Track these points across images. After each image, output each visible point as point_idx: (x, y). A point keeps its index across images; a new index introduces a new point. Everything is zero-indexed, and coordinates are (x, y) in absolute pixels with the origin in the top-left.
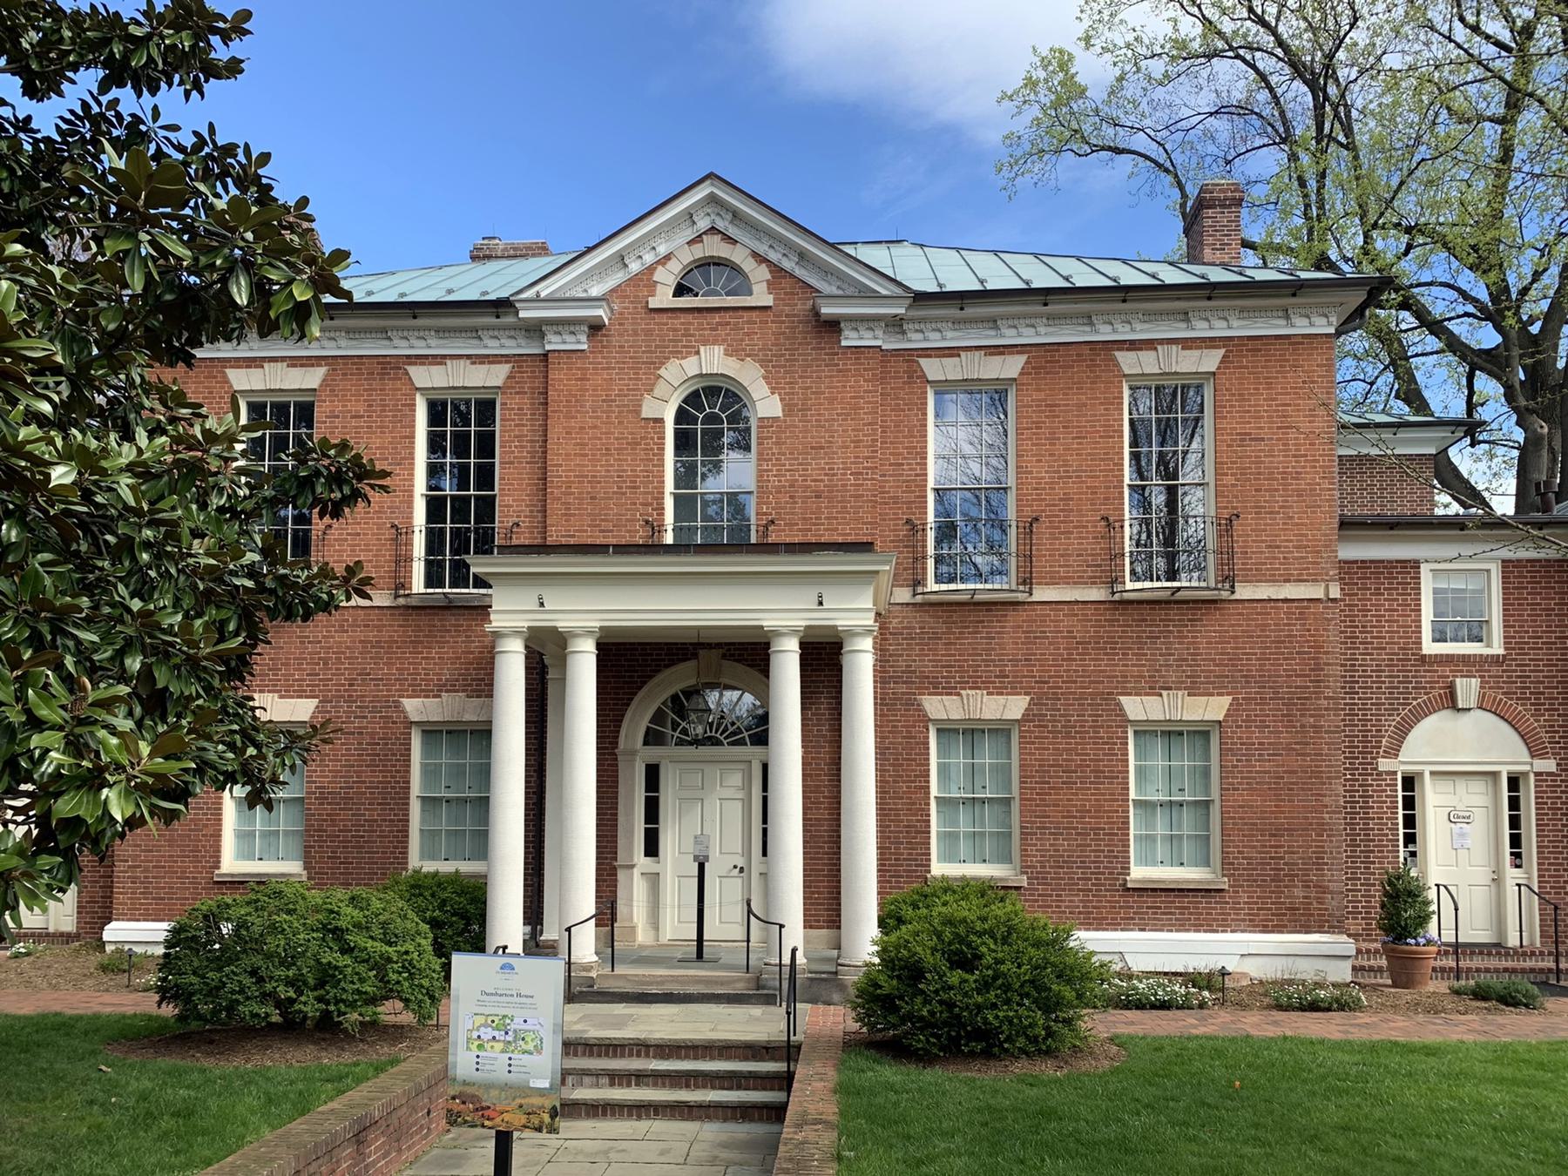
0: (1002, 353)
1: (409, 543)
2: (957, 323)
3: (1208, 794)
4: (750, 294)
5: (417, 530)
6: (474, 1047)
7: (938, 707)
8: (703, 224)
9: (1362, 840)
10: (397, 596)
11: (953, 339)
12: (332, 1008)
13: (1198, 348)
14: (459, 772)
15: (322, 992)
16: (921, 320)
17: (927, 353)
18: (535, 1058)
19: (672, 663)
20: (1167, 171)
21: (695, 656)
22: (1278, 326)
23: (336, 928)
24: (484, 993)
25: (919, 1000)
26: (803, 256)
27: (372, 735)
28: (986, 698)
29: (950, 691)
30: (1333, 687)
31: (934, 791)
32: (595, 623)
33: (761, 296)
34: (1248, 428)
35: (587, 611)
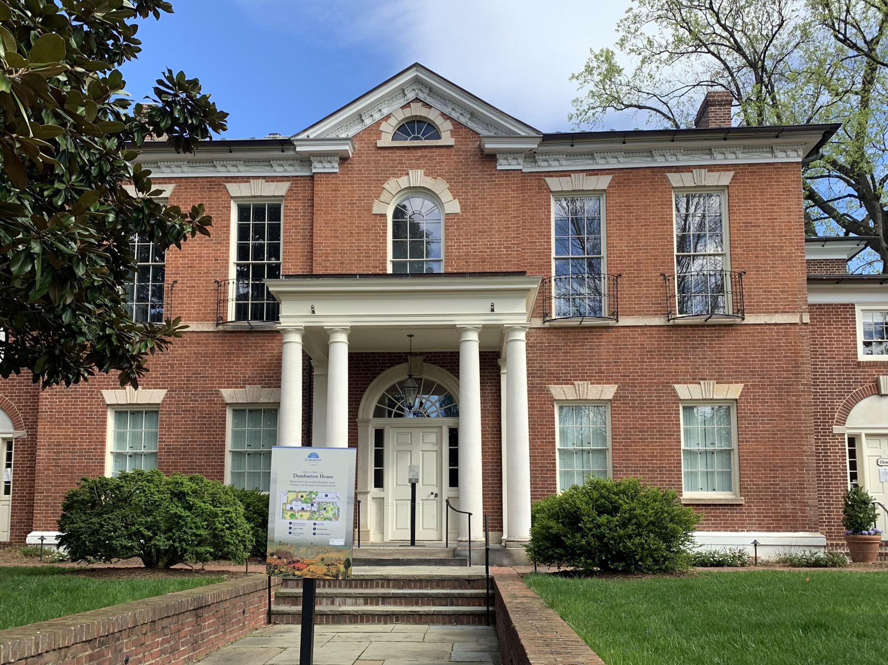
0: (597, 174)
1: (226, 292)
2: (570, 155)
3: (730, 445)
4: (439, 138)
5: (231, 282)
6: (288, 516)
7: (558, 391)
8: (411, 96)
9: (825, 476)
10: (218, 325)
11: (566, 165)
12: (177, 545)
13: (717, 171)
14: (256, 436)
15: (170, 534)
16: (548, 153)
17: (550, 174)
18: (333, 523)
19: (392, 365)
20: (669, 118)
21: (406, 360)
22: (767, 158)
23: (181, 492)
24: (295, 475)
25: (579, 535)
26: (473, 115)
27: (201, 412)
28: (590, 386)
29: (567, 382)
30: (807, 377)
31: (558, 445)
32: (348, 323)
33: (447, 139)
34: (750, 219)
35: (344, 317)
